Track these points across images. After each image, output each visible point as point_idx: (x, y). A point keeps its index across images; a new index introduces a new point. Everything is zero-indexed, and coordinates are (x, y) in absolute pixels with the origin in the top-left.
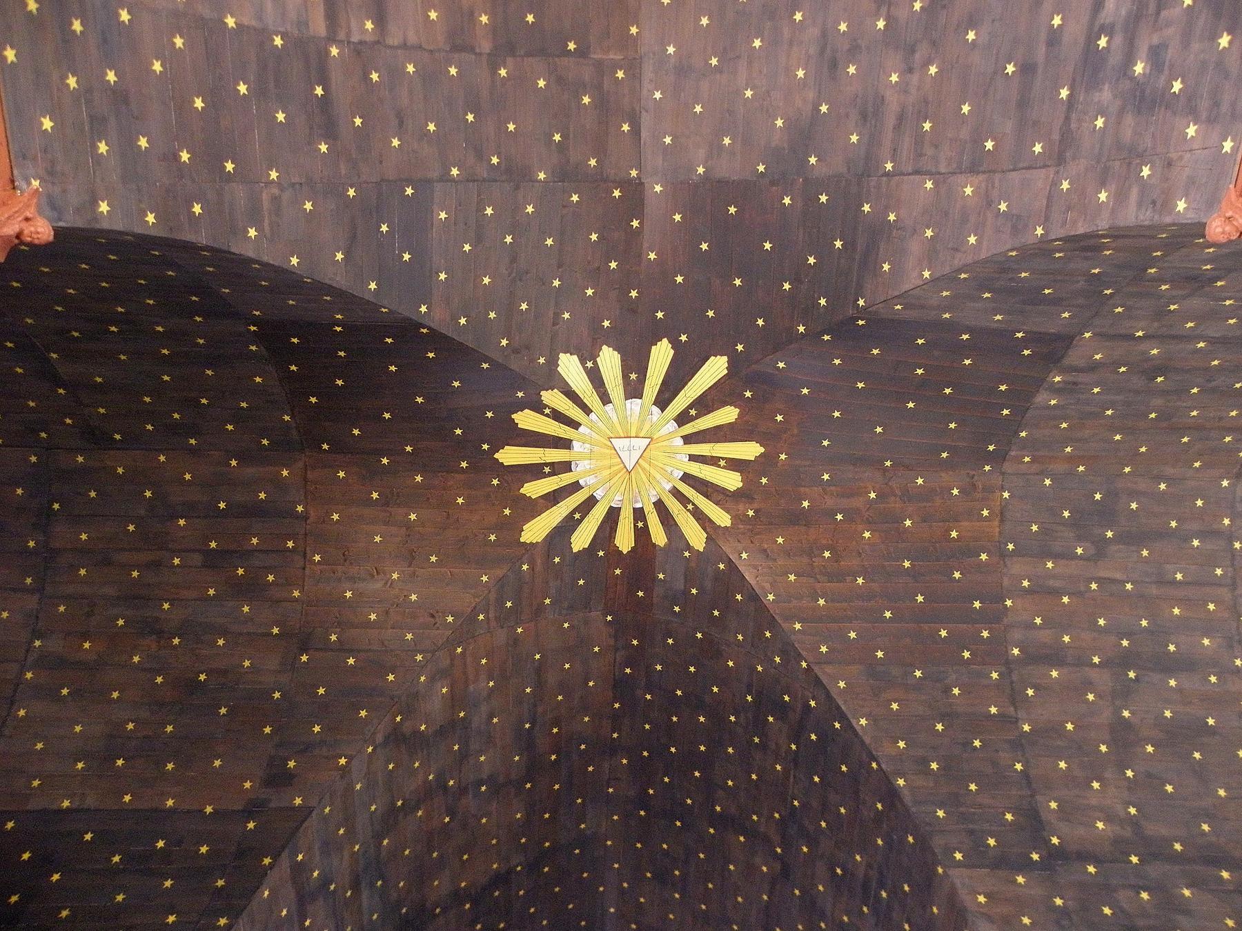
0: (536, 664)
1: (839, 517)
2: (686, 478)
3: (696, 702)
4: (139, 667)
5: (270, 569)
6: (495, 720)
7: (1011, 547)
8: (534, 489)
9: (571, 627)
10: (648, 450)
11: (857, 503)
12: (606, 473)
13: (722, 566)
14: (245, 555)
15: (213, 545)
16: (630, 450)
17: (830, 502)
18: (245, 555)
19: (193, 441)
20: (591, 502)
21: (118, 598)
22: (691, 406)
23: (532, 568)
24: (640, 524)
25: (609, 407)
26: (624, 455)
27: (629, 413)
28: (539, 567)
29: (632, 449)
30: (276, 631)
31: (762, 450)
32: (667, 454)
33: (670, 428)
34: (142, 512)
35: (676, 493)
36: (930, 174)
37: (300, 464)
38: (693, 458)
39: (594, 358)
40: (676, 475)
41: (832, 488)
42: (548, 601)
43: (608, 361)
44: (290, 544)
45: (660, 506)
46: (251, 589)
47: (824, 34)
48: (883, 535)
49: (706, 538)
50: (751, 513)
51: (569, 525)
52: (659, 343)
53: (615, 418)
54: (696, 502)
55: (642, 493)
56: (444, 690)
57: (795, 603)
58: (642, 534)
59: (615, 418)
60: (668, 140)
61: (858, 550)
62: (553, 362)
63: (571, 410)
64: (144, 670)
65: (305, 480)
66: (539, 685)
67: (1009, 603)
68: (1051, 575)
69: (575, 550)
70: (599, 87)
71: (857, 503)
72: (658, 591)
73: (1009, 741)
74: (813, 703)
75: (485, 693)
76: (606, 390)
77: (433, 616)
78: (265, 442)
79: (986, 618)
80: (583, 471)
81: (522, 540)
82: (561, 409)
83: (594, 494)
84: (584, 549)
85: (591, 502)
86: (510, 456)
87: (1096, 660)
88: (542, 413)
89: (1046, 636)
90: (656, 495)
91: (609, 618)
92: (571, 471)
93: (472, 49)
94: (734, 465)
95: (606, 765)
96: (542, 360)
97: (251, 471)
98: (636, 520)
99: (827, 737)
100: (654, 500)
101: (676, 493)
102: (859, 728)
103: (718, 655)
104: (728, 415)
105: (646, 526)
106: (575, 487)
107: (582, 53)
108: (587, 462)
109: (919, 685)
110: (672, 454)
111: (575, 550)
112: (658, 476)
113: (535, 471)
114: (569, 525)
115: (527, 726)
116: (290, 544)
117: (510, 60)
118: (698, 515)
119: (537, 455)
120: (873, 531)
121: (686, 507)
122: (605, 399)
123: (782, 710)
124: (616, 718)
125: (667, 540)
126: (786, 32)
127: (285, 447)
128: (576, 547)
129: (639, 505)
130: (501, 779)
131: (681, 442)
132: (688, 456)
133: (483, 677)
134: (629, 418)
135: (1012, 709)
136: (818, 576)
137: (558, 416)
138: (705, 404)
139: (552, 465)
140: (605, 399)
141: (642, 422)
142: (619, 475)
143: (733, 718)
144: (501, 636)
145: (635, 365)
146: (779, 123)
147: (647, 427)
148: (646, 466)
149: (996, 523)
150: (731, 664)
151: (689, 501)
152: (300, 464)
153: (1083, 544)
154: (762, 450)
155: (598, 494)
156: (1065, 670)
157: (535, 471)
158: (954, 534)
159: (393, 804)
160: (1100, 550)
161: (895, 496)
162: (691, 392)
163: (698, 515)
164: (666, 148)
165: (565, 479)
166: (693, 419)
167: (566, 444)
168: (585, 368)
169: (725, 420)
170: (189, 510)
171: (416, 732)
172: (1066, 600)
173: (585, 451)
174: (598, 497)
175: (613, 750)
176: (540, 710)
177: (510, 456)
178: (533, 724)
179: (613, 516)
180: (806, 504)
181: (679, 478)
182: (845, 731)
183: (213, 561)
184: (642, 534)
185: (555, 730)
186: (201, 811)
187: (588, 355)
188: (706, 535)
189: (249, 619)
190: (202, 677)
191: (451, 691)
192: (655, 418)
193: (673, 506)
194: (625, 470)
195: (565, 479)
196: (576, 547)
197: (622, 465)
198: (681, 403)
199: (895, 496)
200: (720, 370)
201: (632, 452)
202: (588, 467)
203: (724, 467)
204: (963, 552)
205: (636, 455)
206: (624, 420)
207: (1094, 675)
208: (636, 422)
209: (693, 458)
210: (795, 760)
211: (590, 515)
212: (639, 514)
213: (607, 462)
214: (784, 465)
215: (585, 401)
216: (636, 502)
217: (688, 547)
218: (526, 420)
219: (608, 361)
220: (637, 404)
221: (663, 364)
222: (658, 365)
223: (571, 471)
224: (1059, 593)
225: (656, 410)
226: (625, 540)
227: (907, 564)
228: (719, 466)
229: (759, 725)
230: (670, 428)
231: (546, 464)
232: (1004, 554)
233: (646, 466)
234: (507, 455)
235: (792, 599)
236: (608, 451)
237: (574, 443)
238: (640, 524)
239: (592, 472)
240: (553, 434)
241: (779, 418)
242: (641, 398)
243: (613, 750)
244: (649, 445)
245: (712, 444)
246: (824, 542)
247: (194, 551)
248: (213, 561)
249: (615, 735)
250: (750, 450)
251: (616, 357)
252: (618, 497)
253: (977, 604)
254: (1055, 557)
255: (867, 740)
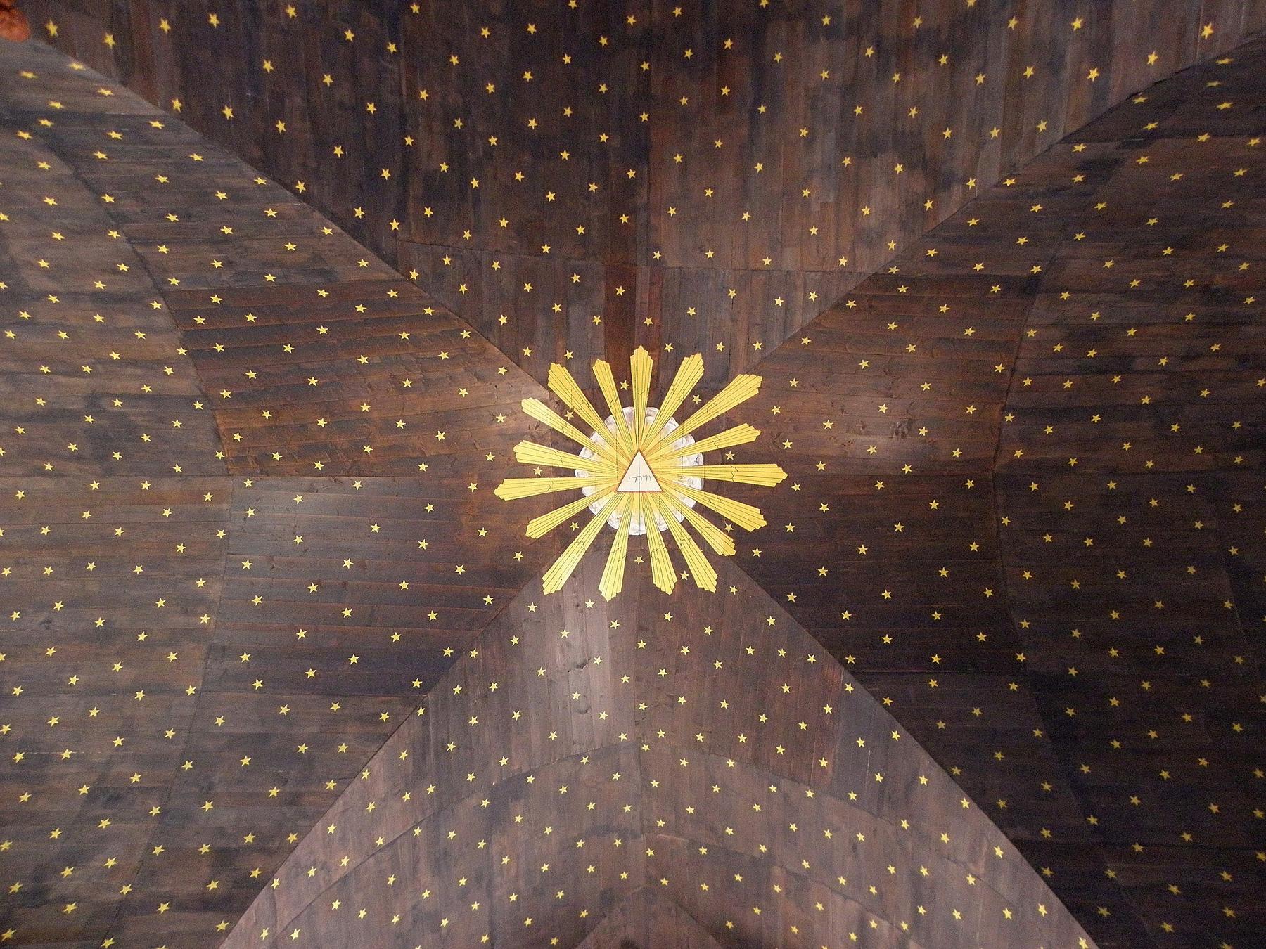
0: (748, 205)
1: (400, 424)
2: (576, 449)
3: (541, 147)
4: (1243, 259)
5: (1058, 356)
6: (804, 132)
7: (198, 405)
8: (745, 434)
9: (703, 251)
10: (620, 478)
11: (382, 440)
12: (665, 451)
13: (527, 352)
14: (1084, 369)
15: (1117, 379)
16: (639, 478)
17: (415, 440)
18: (1084, 369)
19: (1112, 485)
20: (682, 415)
21: (1242, 324)
22: (577, 532)
23: (749, 342)
24: (625, 385)
25: (663, 527)
26: (645, 470)
27: (642, 519)
28: (741, 341)
29: (638, 478)
30: (1065, 296)
31: (497, 492)
32: (599, 474)
33: (597, 505)
34: (1188, 408)
35: (586, 429)
36: (382, 849)
37: (1001, 462)
38: (570, 473)
39: (680, 582)
40: (588, 451)
41: (415, 455)
42: (732, 293)
43: (665, 578)
44: (1028, 382)
45: (604, 411)
46: (1083, 335)
47: (490, 894)
48: (349, 409)
49: (548, 381)
50: (501, 418)
51: (707, 389)
52: (614, 595)
53: (657, 514)
54: (563, 421)
55: (624, 426)
56: (866, 211)
57: (437, 331)
58: (622, 373)
59: (657, 514)
60: (616, 776)
61: (372, 390)
62: (722, 584)
63: (704, 527)
64: (1238, 257)
65: (998, 448)
66: (744, 170)
67: (182, 351)
68: (144, 379)
69: (699, 356)
70: (678, 818)
71: (382, 440)
72: (600, 299)
73: (130, 221)
74: (395, 225)
75: (815, 181)
76: (667, 546)
77: (871, 307)
78: (1034, 486)
79: (207, 335)
80: (688, 453)
81: (760, 378)
82: (715, 529)
83: (677, 425)
84: (689, 356)
85: (682, 415)
86: (769, 475)
87: (54, 299)
88: (735, 525)
89: (124, 321)
90: (608, 424)
91: (657, 255)
92: (704, 454)
93: (788, 872)
94: (525, 471)
95: (656, 16)
96: (734, 590)
97: (1056, 454)
98: (630, 390)
99: (370, 189)
100: (611, 418)
101: (586, 429)
102: (330, 225)
103: (518, 229)
104: (538, 528)
105: (618, 384)
106: (700, 434)
107: (695, 844)
108: (687, 464)
109: (268, 266)
110: (594, 473)
111: (699, 356)
112: (607, 447)
113: (743, 455)
114: (707, 389)
115: (762, 109)
116: (1028, 382)
117: (756, 855)
118: (561, 408)
119: (741, 474)
120: (360, 412)
121: (575, 414)
122: (667, 536)
123: (435, 190)
124: (644, 98)
125: (594, 368)
126: (521, 883)
127: (1014, 479)
128: (697, 358)
129: (627, 410)
130: (800, 27)
131: (586, 491)
132: (576, 474)
133: (816, 208)
134: (642, 514)
135: (139, 251)
136: (414, 360)
137: (717, 520)
138: (563, 537)
139: (725, 462)
140: (667, 536)
141: (628, 512)
142: (650, 447)
143: (493, 141)
144: (791, 259)
145: (638, 572)
146: (519, 819)
147: (623, 504)
148: (621, 459)
149: (222, 428)
150: (504, 223)
151: (571, 422)
152: (1001, 462)
153: (114, 409)
154: (497, 492)
155: (673, 424)
156: (88, 288)
157: (743, 455)
158: (267, 414)
159: (952, 63)
160: (94, 402)
161: (343, 450)
162: (578, 549)
163: (561, 408)
164: (618, 770)
165: (710, 444)
166: (574, 518)
167: (711, 486)
168: (689, 572)
169: (538, 523)
170: (1137, 412)
171: (909, 166)
172: (115, 356)
173: (688, 477)
174: (673, 420)
175: (649, 42)
176: (744, 131)
177: (769, 475)
178: (754, 111)
179: (656, 398)
180: (441, 436)
181: (584, 449)
182: (348, 209)
183: (1123, 363)
184: (622, 373)
185: (725, 91)
186: (1214, 135)
187: (687, 585)
188: (549, 385)
189: (1094, 307)
190: (1168, 251)
191: (857, 206)
192: (614, 514)
193: (588, 414)
194: (644, 453)
195: (710, 444)
196: (697, 358)
197: (647, 459)
198: (587, 536)
199: (343, 450)
200: (549, 580)
201: (636, 475)
202: (685, 458)
203: (535, 466)
204: (248, 398)
205: (633, 471)
206: (646, 510)
207: (51, 285)
208: (634, 509)
209: (570, 473)
210: (404, 124)
211: (682, 399)
212: (626, 399)
213: (665, 463)
214: (471, 476)
215: (689, 536)
216: (630, 414)
217: (567, 364)
218: (751, 518)
219: (665, 578)
220: (634, 529)
221: (609, 575)
222: (614, 571)
223: (704, 454)
224: (123, 362)
225: (614, 525)
226: (642, 363)
227: (313, 381)
228: (541, 467)
229: (458, 148)
230: (597, 505)
231: (730, 462)
232: (204, 398)
233: (621, 459)
234: (772, 475)
235: (441, 335)
236: (663, 476)
237: (700, 486)
238: (625, 385)
239: (680, 453)
240: (723, 498)
241: (483, 533)
242: (630, 536)
243: (649, 42)
244: (619, 485)
245: (551, 491)
246: (413, 396)
247: (1143, 372)
248: (1123, 363)
249: (645, 66)
250: (510, 490)
251: (657, 581)
252: (651, 419)
253: (219, 348)
254: (143, 396)
255: (317, 215)
